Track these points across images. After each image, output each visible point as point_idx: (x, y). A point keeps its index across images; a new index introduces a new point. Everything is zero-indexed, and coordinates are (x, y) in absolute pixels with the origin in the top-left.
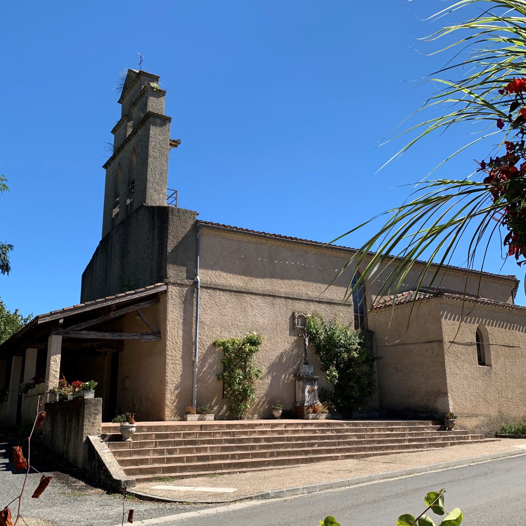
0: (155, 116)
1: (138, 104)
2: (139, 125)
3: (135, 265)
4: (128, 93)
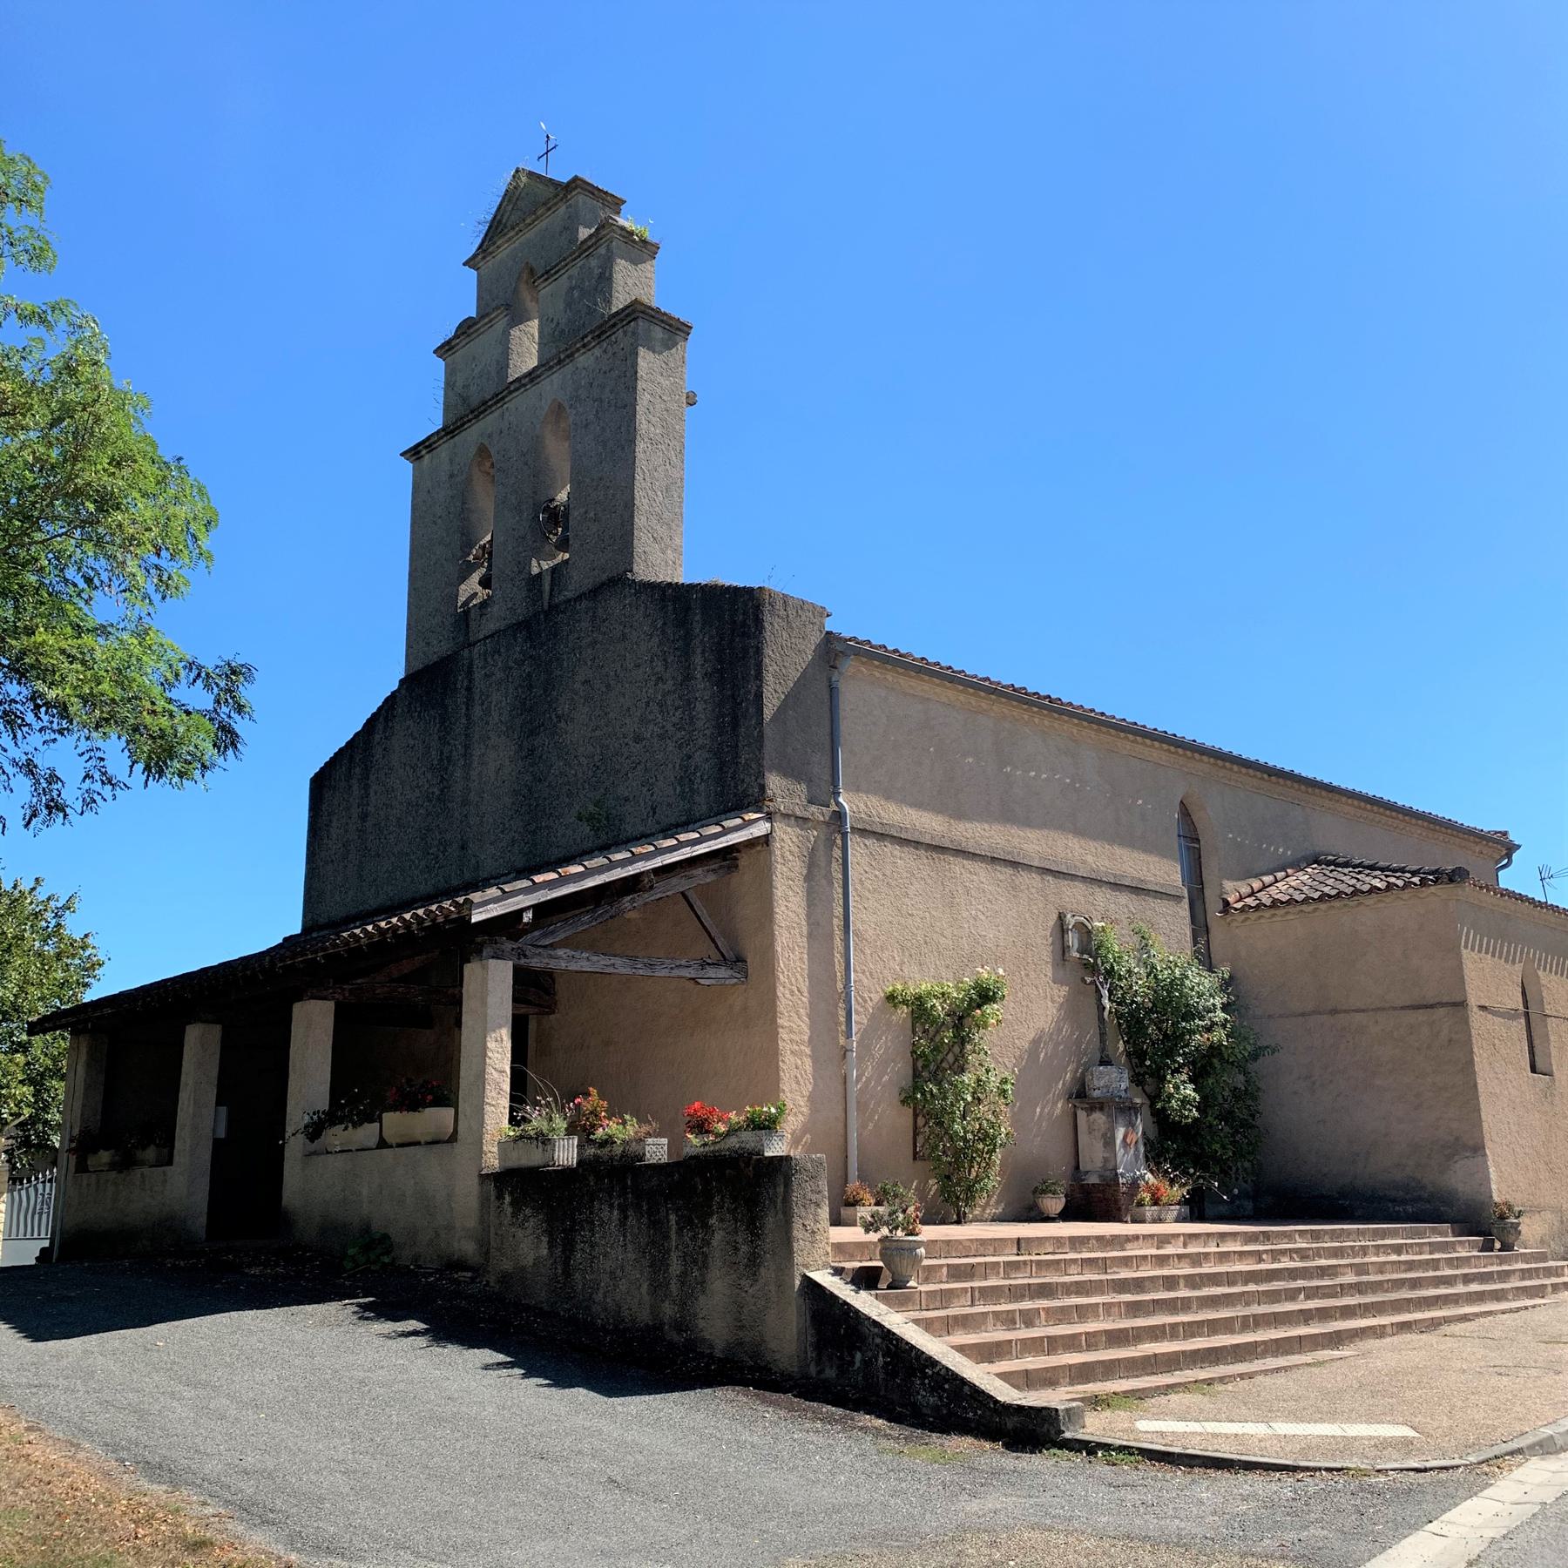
2: (589, 338)
4: (510, 239)
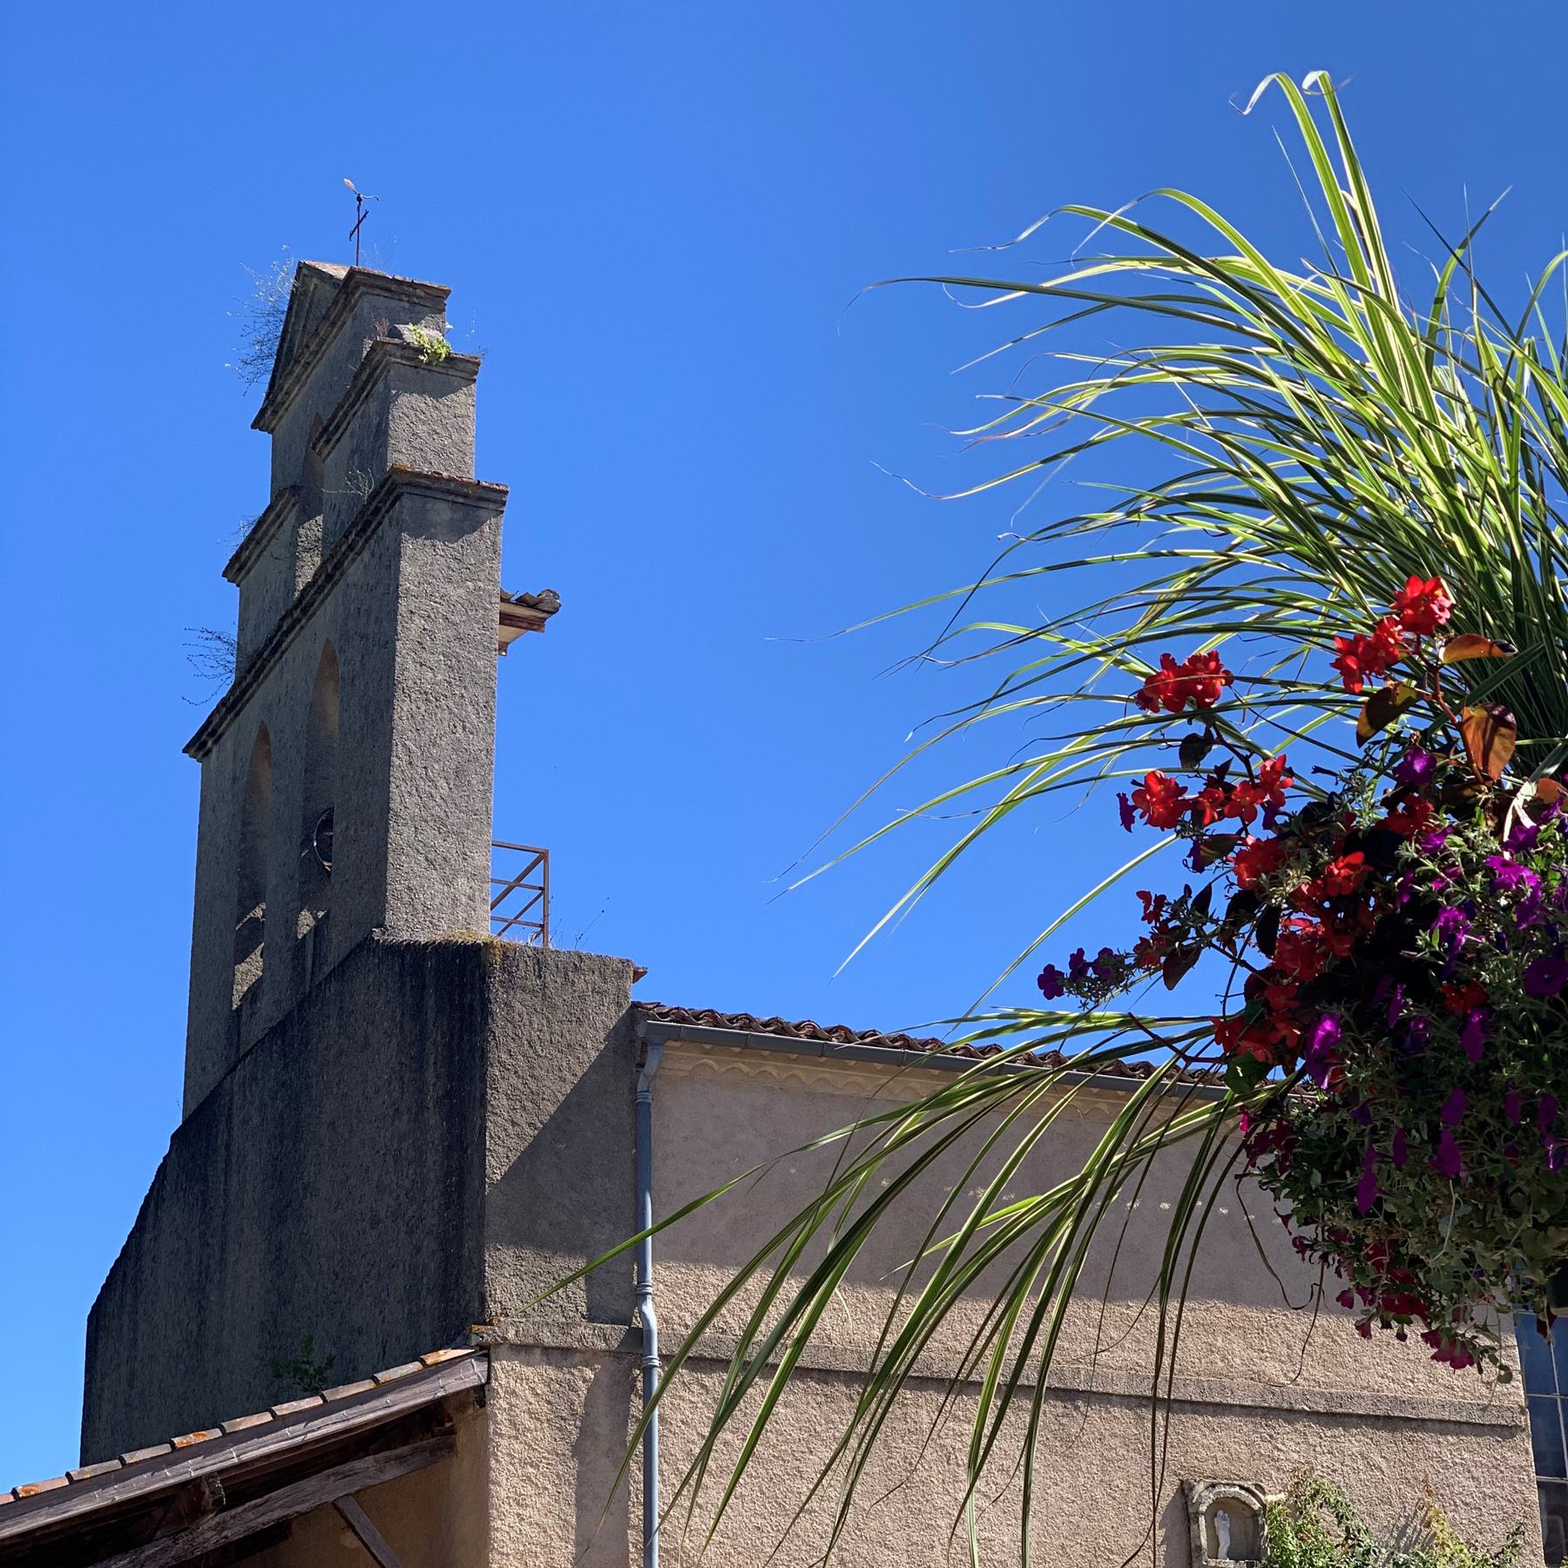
0: (428, 488)
1: (348, 431)
2: (352, 536)
3: (338, 1257)
4: (298, 378)
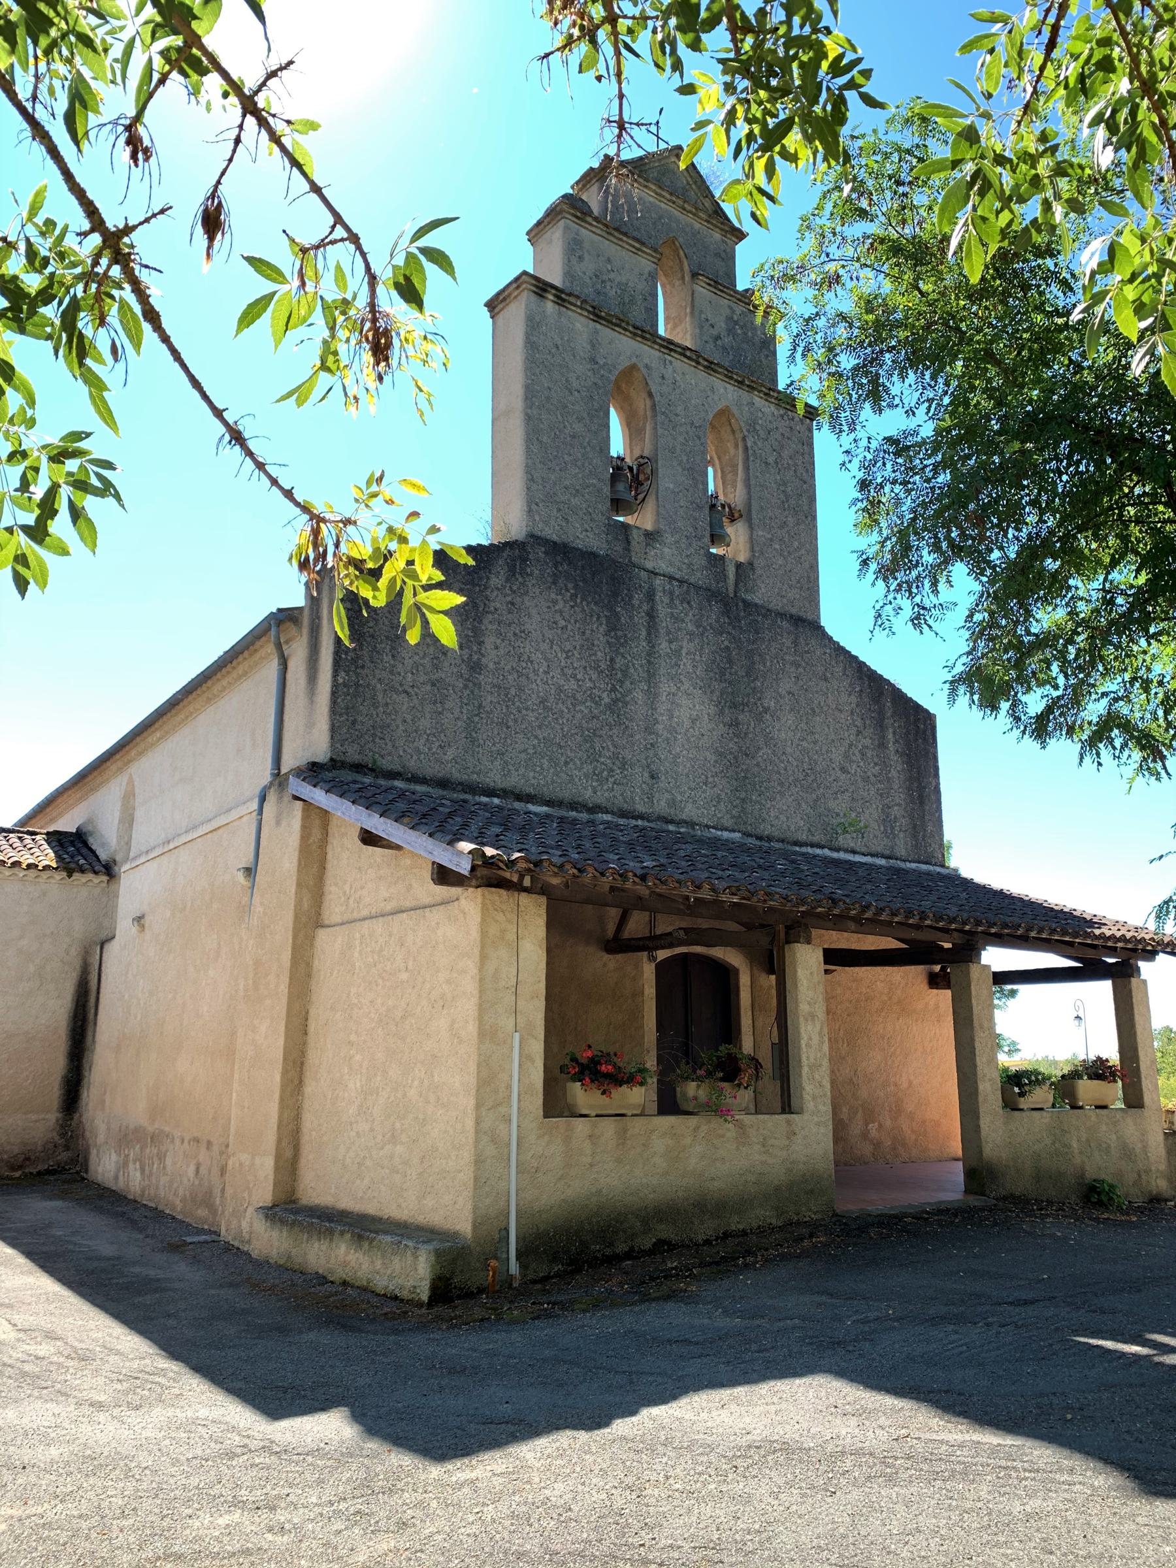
4: (660, 195)
